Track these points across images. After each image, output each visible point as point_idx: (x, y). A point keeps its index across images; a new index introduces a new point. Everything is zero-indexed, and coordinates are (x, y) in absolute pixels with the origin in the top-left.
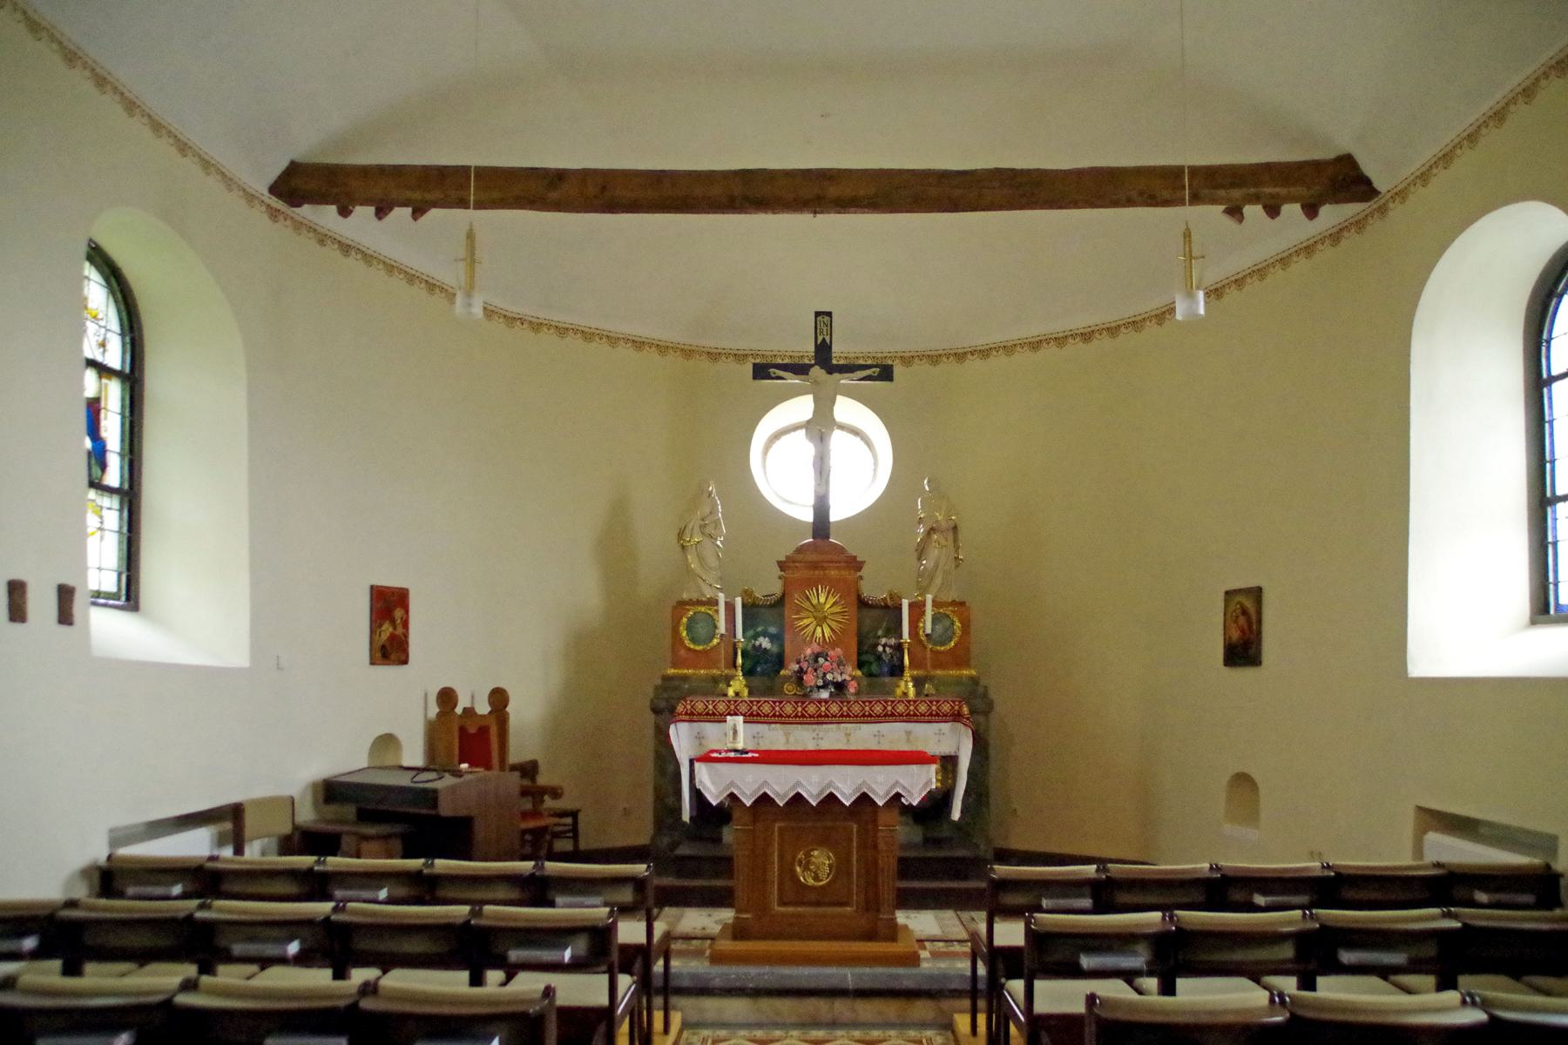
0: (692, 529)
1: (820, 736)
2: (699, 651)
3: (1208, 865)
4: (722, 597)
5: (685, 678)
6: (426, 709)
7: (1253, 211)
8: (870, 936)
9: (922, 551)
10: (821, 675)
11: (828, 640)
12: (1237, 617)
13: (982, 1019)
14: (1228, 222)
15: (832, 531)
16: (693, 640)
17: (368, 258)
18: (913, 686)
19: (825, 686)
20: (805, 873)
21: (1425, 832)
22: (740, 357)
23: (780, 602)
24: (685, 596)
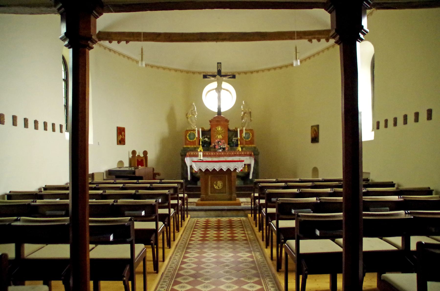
2: (191, 142)
4: (196, 129)
5: (188, 148)
7: (314, 41)
10: (219, 146)
12: (314, 132)
13: (253, 215)
14: (309, 43)
15: (222, 113)
16: (190, 139)
17: (115, 52)
18: (241, 148)
19: (220, 149)
22: (200, 73)
23: (210, 130)
24: (188, 129)
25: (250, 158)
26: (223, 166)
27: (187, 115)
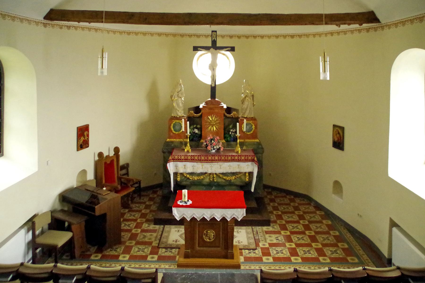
0: (175, 96)
1: (212, 166)
3: (328, 269)
5: (172, 142)
6: (94, 158)
8: (226, 257)
9: (243, 102)
11: (215, 131)
16: (175, 130)
20: (206, 238)
21: (393, 227)
25: (252, 164)
26: (216, 215)
27: (171, 97)
